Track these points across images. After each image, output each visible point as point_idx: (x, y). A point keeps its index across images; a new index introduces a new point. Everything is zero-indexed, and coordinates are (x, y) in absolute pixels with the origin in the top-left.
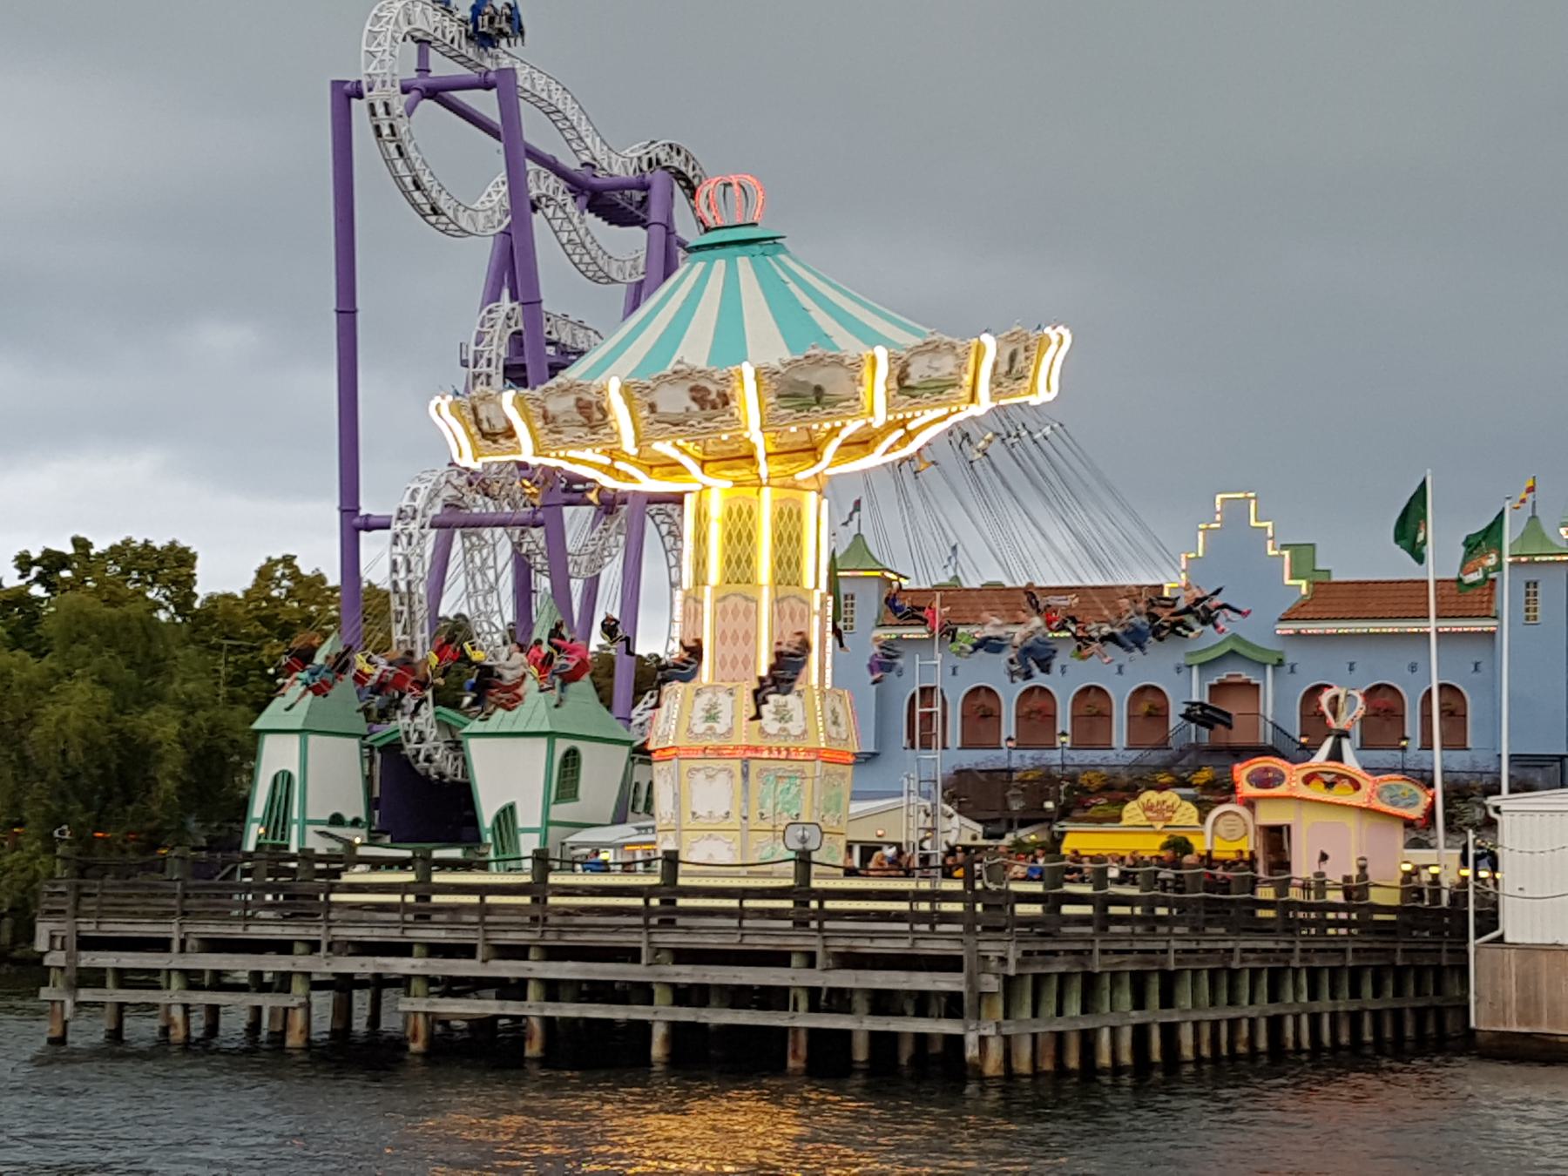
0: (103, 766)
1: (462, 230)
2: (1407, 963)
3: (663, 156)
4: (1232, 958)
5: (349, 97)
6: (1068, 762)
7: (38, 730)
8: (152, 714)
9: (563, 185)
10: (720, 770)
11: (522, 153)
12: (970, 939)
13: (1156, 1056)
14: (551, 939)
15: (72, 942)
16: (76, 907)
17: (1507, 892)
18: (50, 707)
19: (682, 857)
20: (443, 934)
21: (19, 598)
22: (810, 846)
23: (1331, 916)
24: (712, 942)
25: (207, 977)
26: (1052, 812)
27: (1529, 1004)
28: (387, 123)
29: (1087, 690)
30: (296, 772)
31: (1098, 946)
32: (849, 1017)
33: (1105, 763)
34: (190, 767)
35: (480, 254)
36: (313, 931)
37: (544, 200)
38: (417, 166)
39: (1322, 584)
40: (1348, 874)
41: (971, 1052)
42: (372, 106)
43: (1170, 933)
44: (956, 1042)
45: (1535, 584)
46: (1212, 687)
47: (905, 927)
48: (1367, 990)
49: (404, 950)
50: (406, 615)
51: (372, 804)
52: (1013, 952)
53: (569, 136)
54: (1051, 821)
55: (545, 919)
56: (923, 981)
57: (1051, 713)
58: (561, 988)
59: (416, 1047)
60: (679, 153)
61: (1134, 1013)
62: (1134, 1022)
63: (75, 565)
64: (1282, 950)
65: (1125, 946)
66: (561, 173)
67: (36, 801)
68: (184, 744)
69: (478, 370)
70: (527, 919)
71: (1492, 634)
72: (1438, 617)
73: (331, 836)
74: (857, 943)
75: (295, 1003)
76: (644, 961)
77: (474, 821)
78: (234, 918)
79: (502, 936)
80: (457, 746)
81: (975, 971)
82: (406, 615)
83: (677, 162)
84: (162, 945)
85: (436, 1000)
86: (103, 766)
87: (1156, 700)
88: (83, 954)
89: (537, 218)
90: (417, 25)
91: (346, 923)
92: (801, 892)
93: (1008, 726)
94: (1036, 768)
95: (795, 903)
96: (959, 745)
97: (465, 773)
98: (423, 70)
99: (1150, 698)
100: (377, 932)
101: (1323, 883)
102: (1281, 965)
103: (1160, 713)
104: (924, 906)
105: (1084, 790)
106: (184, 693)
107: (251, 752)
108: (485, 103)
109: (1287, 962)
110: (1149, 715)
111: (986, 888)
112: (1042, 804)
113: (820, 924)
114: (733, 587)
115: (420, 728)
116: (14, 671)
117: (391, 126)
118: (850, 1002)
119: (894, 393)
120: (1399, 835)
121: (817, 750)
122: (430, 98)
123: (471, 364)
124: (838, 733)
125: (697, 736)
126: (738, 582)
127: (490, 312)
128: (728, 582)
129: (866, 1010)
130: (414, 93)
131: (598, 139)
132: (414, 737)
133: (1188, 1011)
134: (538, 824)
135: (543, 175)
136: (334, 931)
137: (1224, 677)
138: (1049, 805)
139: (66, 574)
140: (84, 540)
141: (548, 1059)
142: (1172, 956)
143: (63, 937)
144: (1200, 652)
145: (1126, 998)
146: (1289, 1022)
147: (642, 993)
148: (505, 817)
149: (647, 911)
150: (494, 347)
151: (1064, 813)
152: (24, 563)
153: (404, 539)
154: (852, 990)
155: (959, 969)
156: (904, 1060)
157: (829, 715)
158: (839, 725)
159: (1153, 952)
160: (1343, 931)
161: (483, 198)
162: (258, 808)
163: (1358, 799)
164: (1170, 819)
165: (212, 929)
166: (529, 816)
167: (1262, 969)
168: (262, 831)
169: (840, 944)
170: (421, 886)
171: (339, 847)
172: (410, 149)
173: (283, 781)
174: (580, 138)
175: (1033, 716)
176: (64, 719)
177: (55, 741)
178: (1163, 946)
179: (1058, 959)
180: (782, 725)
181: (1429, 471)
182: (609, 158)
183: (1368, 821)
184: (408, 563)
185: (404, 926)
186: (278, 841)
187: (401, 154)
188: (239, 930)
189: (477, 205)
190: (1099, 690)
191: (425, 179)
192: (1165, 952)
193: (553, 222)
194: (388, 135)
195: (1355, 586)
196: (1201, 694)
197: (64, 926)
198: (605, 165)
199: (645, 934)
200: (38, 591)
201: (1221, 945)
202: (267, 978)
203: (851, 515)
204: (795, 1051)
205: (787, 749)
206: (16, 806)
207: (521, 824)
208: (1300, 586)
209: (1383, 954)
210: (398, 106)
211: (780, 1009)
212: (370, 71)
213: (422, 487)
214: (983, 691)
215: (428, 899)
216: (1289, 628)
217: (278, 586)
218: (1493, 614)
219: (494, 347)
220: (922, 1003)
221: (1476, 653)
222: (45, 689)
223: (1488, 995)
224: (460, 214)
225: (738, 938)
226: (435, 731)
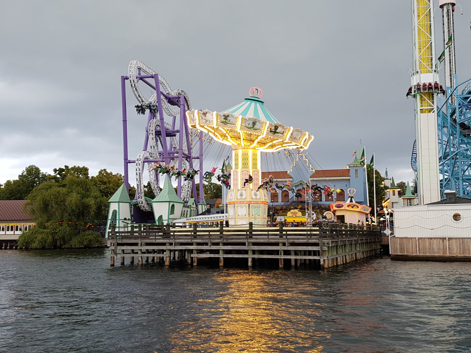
0: (79, 209)
3: (180, 92)
5: (125, 79)
8: (89, 199)
9: (164, 97)
19: (253, 223)
20: (200, 241)
24: (262, 241)
27: (402, 249)
28: (134, 84)
30: (117, 210)
41: (322, 263)
44: (319, 260)
45: (357, 170)
46: (297, 190)
47: (306, 237)
49: (191, 244)
53: (164, 88)
56: (310, 248)
63: (65, 171)
68: (95, 204)
69: (150, 132)
70: (219, 237)
71: (350, 179)
73: (124, 222)
74: (295, 240)
76: (247, 245)
79: (214, 241)
81: (322, 246)
85: (199, 254)
86: (79, 209)
87: (287, 193)
88: (118, 247)
97: (152, 209)
98: (139, 74)
100: (185, 240)
104: (309, 233)
107: (108, 206)
110: (285, 196)
114: (244, 169)
117: (134, 85)
119: (269, 131)
126: (245, 168)
128: (243, 168)
129: (252, 253)
130: (138, 79)
134: (167, 219)
136: (175, 241)
139: (64, 173)
141: (254, 267)
143: (114, 243)
144: (295, 184)
147: (246, 252)
148: (160, 218)
149: (247, 235)
152: (55, 170)
153: (138, 165)
154: (291, 250)
155: (319, 246)
161: (150, 99)
163: (358, 210)
164: (296, 215)
166: (165, 217)
169: (291, 241)
170: (195, 231)
173: (115, 212)
178: (345, 240)
180: (256, 197)
183: (360, 214)
185: (192, 239)
187: (136, 90)
191: (141, 95)
192: (345, 241)
195: (345, 171)
197: (114, 241)
200: (58, 176)
202: (150, 251)
203: (227, 159)
204: (281, 264)
210: (136, 81)
211: (277, 255)
212: (130, 74)
213: (141, 154)
215: (196, 233)
221: (346, 183)
226: (145, 201)
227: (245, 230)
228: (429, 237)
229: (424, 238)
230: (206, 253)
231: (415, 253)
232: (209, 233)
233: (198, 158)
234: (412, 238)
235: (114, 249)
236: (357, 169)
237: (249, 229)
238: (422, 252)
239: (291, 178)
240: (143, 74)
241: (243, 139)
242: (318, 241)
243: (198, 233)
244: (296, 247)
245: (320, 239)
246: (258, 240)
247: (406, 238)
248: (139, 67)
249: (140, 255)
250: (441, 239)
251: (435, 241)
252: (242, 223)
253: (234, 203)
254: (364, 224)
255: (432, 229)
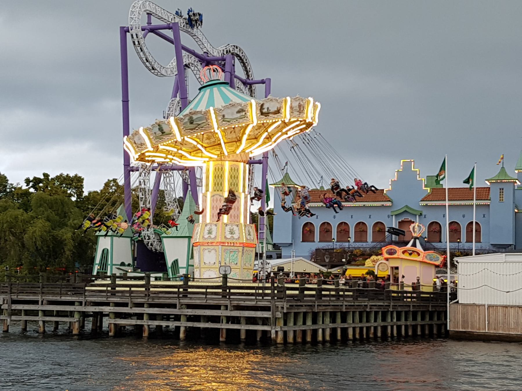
0: (48, 247)
1: (162, 74)
2: (434, 310)
3: (231, 49)
4: (367, 308)
6: (350, 246)
7: (26, 235)
8: (63, 230)
9: (197, 59)
10: (212, 250)
11: (181, 48)
12: (273, 301)
13: (339, 337)
14: (150, 301)
15: (9, 301)
16: (11, 291)
17: (460, 288)
18: (30, 228)
20: (119, 299)
21: (26, 193)
22: (227, 273)
23: (405, 295)
24: (198, 302)
25: (55, 313)
26: (345, 263)
27: (465, 322)
28: (137, 40)
29: (359, 223)
31: (317, 304)
32: (239, 325)
33: (362, 246)
34: (75, 247)
35: (171, 82)
36: (81, 298)
37: (191, 64)
38: (147, 54)
39: (435, 189)
40: (414, 282)
41: (273, 336)
42: (132, 35)
43: (344, 300)
45: (503, 190)
46: (399, 222)
47: (254, 297)
48: (419, 318)
49: (107, 304)
50: (144, 199)
51: (134, 259)
52: (286, 305)
53: (199, 44)
54: (344, 265)
55: (149, 295)
57: (348, 230)
58: (157, 316)
59: (111, 334)
60: (237, 48)
61: (331, 324)
62: (331, 327)
64: (386, 306)
65: (327, 304)
66: (197, 56)
67: (27, 258)
68: (73, 240)
70: (144, 295)
71: (489, 205)
72: (476, 200)
73: (121, 269)
75: (75, 320)
76: (177, 308)
77: (165, 264)
78: (68, 295)
79: (136, 300)
80: (160, 241)
82: (144, 199)
83: (236, 51)
84: (36, 302)
86: (48, 247)
88: (13, 305)
89: (189, 70)
90: (147, 9)
91: (90, 296)
92: (224, 287)
93: (334, 235)
94: (340, 248)
95: (223, 291)
96: (318, 241)
98: (149, 23)
99: (379, 226)
100: (99, 299)
101: (403, 285)
102: (386, 310)
103: (383, 231)
104: (261, 291)
105: (356, 256)
106: (74, 224)
108: (169, 33)
109: (388, 309)
110: (379, 231)
111: (278, 286)
112: (341, 260)
113: (229, 297)
114: (217, 192)
115: (149, 235)
116: (19, 216)
117: (138, 42)
118: (240, 320)
120: (433, 270)
121: (243, 243)
122: (151, 32)
123: (166, 117)
124: (250, 238)
125: (206, 239)
126: (218, 191)
127: (173, 101)
128: (215, 191)
130: (146, 31)
131: (209, 44)
132: (147, 238)
133: (351, 324)
134: (185, 266)
135: (190, 56)
136: (87, 299)
137: (403, 219)
138: (344, 260)
139: (41, 185)
140: (47, 174)
142: (344, 307)
145: (328, 320)
146: (389, 328)
147: (177, 318)
149: (179, 293)
150: (173, 112)
151: (349, 263)
152: (28, 181)
154: (240, 317)
155: (270, 311)
156: (258, 339)
157: (247, 232)
158: (250, 235)
159: (338, 305)
160: (409, 300)
161: (170, 64)
162: (98, 260)
163: (419, 258)
165: (51, 298)
167: (379, 311)
168: (99, 267)
169: (235, 303)
170: (112, 285)
171: (122, 272)
172: (144, 49)
174: (203, 44)
175: (342, 231)
176: (34, 232)
177: (32, 239)
178: (341, 304)
179: (304, 307)
180: (232, 235)
181: (446, 155)
182: (213, 50)
183: (423, 265)
184: (144, 181)
186: (104, 271)
187: (142, 51)
188: (59, 298)
189: (168, 66)
190: (363, 223)
191: (150, 59)
192: (342, 306)
193: (194, 71)
194: (137, 44)
195: (482, 189)
196: (396, 225)
197: (7, 297)
198: (212, 53)
199: (178, 299)
200: (32, 190)
201: (363, 304)
203: (285, 167)
205: (234, 243)
206: (20, 260)
207: (180, 266)
208: (428, 190)
209: (424, 307)
212: (131, 24)
214: (326, 223)
215: (115, 289)
216: (424, 203)
217: (111, 188)
218: (489, 199)
219: (173, 112)
220: (167, 317)
222: (29, 222)
223: (453, 319)
224: (162, 69)
225: (205, 301)
226: (154, 236)
227: (177, 285)
228: (502, 304)
229: (497, 306)
230: (133, 318)
231: (483, 329)
232: (130, 289)
233: (260, 162)
234: (479, 306)
235: (7, 308)
236: (501, 187)
237: (110, 284)
238: (493, 327)
239: (389, 201)
240: (155, 22)
241: (225, 143)
242: (269, 303)
243: (117, 289)
244: (241, 312)
245: (271, 301)
246: (193, 301)
247: (474, 305)
248: (148, 12)
249: (40, 318)
250: (520, 307)
251: (512, 310)
252: (210, 276)
253: (203, 244)
254: (420, 281)
255: (507, 292)
